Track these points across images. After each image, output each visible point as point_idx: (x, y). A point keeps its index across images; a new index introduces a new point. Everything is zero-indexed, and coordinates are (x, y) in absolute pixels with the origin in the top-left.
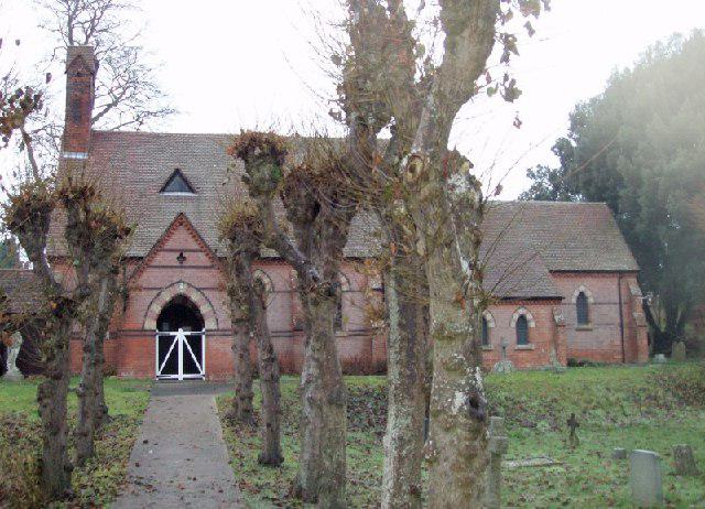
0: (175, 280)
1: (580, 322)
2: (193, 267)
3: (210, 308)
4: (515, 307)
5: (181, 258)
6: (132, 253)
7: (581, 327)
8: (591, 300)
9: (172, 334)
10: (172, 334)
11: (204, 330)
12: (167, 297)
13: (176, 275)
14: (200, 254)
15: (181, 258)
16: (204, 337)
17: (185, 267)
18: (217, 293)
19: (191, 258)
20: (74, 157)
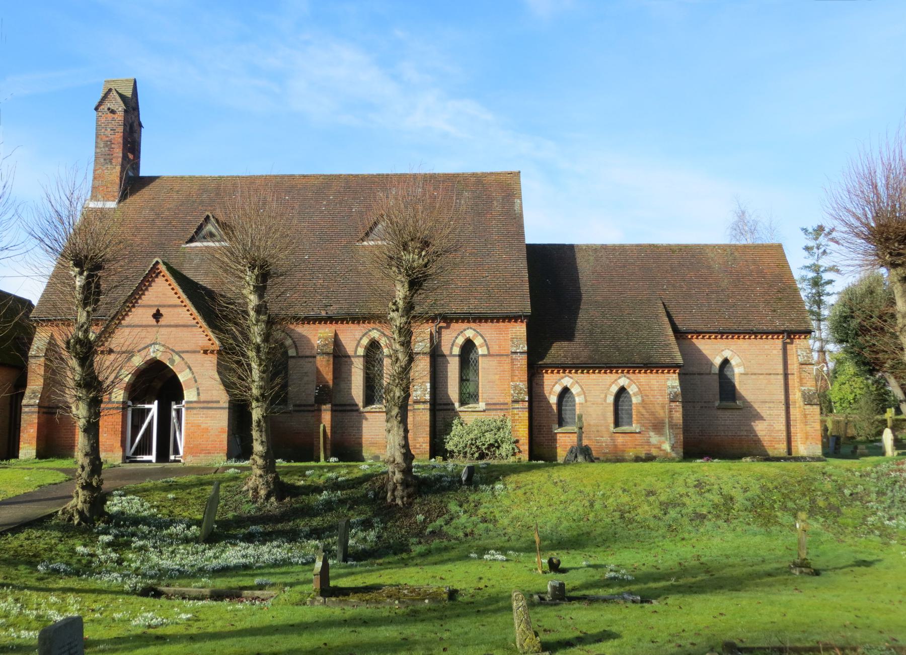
0: (149, 342)
1: (721, 399)
2: (176, 326)
3: (190, 376)
4: (614, 376)
5: (157, 316)
6: (522, 432)
7: (725, 404)
8: (481, 351)
9: (147, 406)
10: (147, 406)
11: (184, 402)
12: (138, 361)
13: (149, 336)
14: (180, 310)
15: (157, 316)
16: (183, 409)
17: (156, 306)
18: (201, 356)
19: (168, 316)
20: (255, 434)
